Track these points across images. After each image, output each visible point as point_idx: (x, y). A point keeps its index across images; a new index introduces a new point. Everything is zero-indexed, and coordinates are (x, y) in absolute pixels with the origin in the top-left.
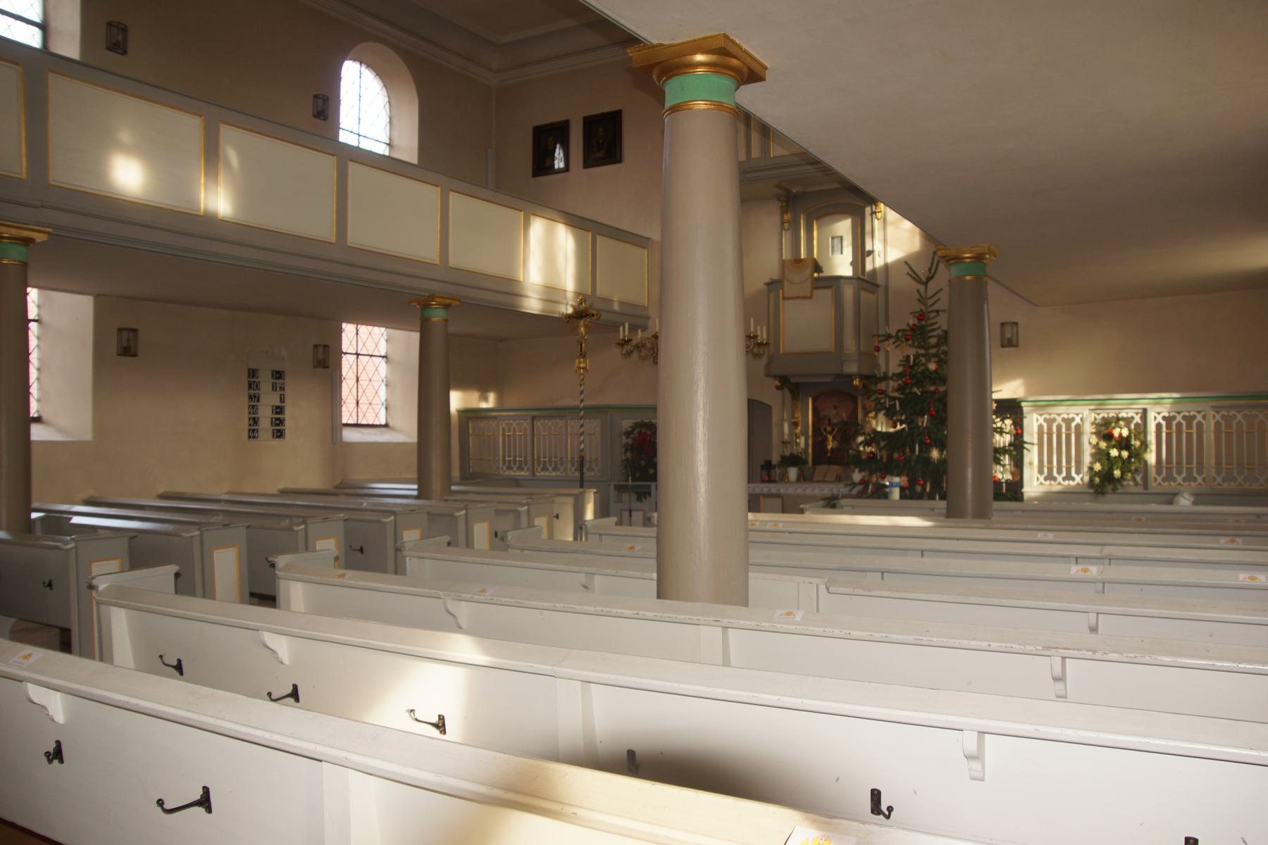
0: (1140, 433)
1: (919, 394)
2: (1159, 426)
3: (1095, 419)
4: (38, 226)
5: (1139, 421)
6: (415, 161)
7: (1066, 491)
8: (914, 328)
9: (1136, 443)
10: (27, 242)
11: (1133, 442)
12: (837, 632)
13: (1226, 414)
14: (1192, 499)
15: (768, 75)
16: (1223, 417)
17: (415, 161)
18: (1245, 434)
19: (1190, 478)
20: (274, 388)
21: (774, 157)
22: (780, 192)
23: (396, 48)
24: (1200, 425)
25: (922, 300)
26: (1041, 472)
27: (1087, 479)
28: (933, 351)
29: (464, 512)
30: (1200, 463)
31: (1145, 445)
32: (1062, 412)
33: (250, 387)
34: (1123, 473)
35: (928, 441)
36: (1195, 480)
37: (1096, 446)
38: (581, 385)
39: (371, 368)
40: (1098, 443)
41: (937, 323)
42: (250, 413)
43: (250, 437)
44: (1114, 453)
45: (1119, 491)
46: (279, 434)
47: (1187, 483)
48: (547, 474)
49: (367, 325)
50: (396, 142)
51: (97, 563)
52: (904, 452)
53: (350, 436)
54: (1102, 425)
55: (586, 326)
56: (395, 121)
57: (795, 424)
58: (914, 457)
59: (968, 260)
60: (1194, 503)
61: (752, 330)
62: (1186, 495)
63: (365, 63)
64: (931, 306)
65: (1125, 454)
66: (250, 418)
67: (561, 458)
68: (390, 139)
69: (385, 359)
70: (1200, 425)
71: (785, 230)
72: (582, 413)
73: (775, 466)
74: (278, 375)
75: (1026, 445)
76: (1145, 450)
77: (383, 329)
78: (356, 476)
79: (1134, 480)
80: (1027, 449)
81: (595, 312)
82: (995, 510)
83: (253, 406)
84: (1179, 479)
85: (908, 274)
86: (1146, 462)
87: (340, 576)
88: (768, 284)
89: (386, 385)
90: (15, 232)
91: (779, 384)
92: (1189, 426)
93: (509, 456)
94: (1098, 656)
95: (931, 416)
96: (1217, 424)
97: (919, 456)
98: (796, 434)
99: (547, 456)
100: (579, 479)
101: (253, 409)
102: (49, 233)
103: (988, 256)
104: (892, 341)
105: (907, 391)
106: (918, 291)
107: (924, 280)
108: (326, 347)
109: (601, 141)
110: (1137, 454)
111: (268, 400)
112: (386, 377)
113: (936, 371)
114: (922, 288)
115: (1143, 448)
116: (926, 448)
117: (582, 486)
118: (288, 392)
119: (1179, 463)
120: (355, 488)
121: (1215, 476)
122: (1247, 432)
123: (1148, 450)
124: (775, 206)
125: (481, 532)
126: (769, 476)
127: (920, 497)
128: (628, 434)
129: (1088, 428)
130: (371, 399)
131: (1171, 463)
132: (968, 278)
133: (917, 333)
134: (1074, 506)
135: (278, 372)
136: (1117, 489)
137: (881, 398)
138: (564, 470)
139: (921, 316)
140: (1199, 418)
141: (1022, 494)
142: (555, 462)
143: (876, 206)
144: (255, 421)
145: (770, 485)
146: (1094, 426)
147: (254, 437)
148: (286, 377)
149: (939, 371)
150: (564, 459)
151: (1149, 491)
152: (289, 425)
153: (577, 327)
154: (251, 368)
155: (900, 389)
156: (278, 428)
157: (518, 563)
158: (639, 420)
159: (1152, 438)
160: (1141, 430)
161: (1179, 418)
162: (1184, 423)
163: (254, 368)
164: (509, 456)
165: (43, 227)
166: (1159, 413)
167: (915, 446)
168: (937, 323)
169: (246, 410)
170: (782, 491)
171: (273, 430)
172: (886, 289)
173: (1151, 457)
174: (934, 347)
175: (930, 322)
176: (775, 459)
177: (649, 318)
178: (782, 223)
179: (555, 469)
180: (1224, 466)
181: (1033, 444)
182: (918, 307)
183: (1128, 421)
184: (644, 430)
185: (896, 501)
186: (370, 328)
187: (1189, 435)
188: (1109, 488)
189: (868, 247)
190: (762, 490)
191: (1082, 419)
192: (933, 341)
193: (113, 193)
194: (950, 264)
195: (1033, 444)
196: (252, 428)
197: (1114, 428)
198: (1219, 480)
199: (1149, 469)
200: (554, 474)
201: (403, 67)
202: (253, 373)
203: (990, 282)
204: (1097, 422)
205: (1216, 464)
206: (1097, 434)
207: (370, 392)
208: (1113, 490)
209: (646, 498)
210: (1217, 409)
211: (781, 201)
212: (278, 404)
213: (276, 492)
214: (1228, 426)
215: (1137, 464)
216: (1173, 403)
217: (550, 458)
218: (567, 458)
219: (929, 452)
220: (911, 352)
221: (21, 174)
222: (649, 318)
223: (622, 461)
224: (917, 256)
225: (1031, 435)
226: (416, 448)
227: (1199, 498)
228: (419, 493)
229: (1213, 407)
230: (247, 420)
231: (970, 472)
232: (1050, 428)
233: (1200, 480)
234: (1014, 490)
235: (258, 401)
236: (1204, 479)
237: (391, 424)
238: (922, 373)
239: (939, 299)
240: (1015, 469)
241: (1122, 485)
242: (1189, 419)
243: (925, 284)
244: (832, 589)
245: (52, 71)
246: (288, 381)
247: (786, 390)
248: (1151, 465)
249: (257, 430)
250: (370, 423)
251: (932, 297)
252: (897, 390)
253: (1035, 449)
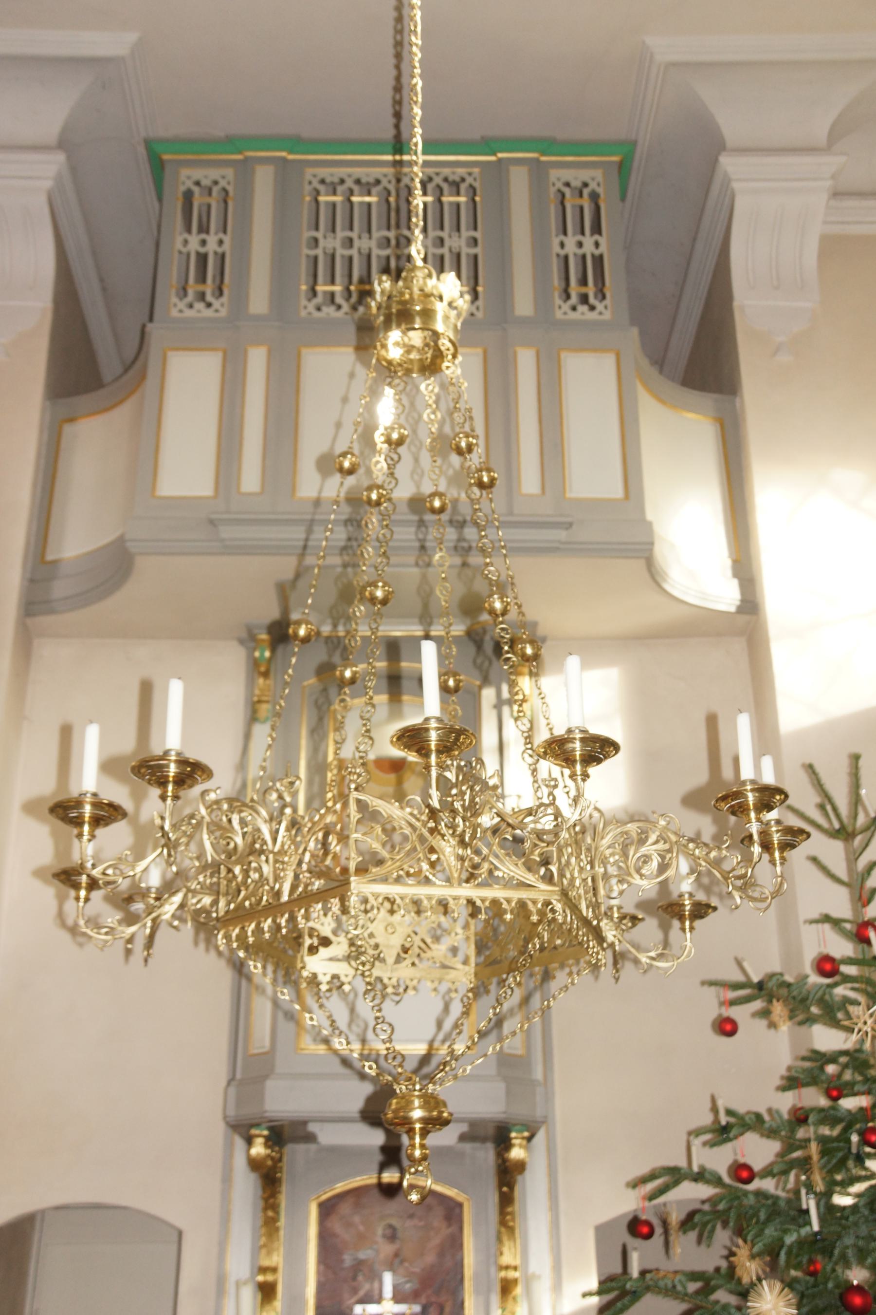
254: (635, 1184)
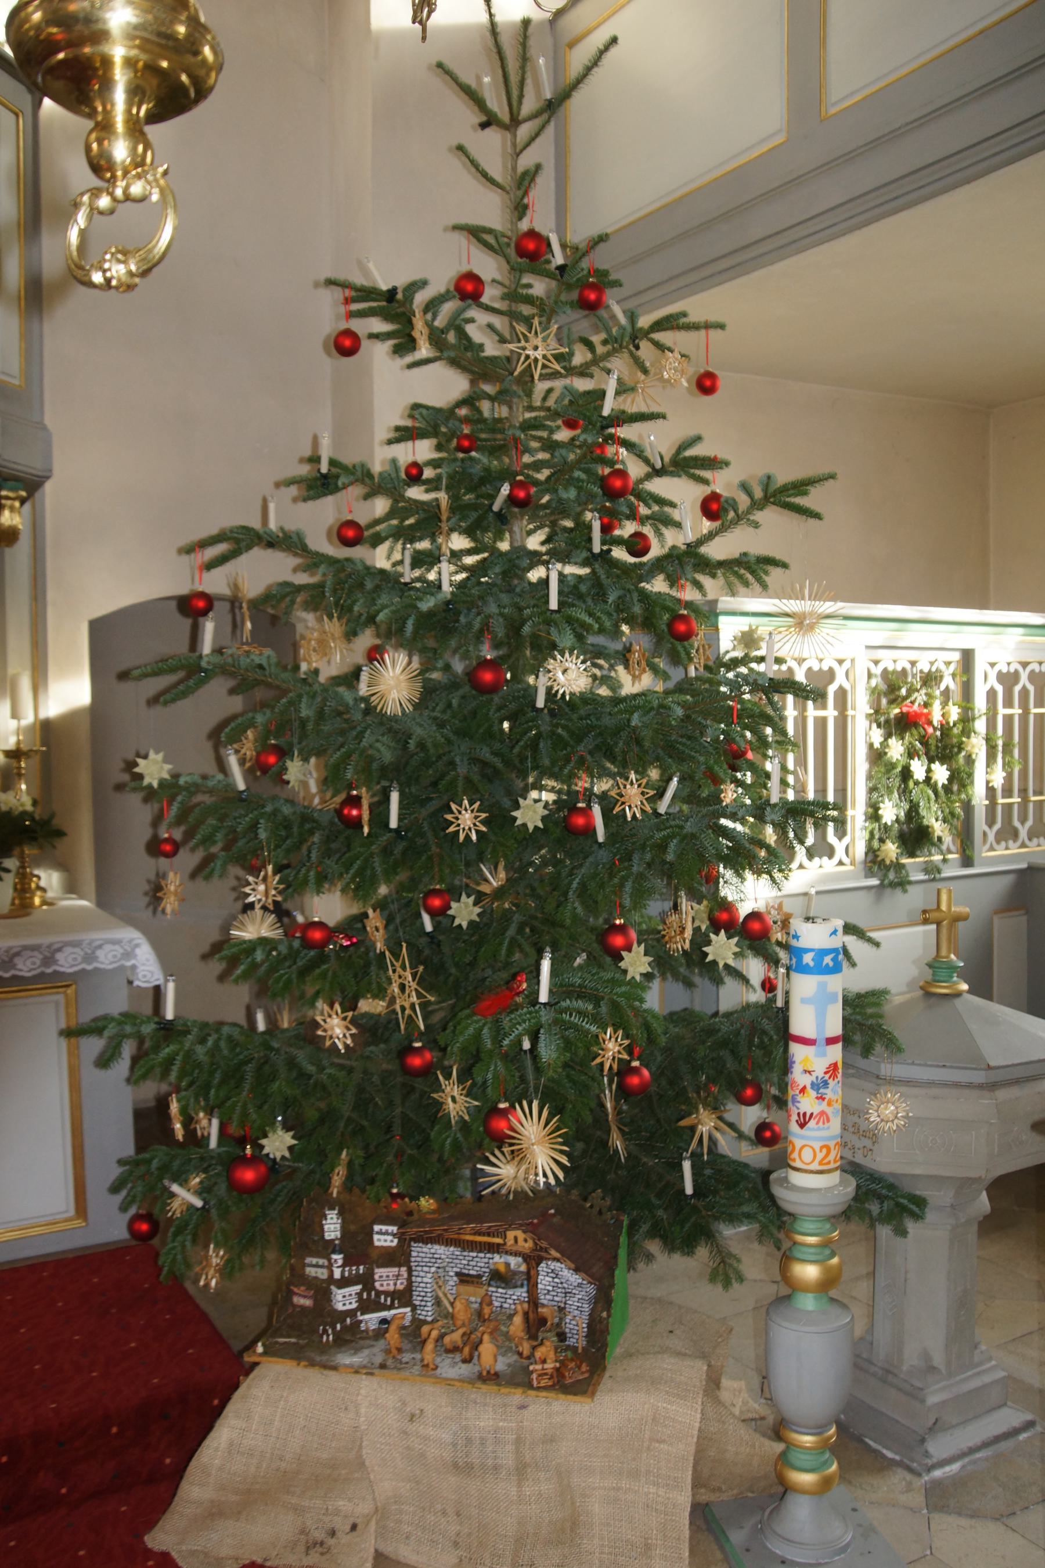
2: (991, 694)
27: (860, 850)
37: (877, 756)
40: (884, 744)
129: (861, 706)
166: (992, 665)
204: (874, 682)
206: (876, 716)
254: (189, 550)
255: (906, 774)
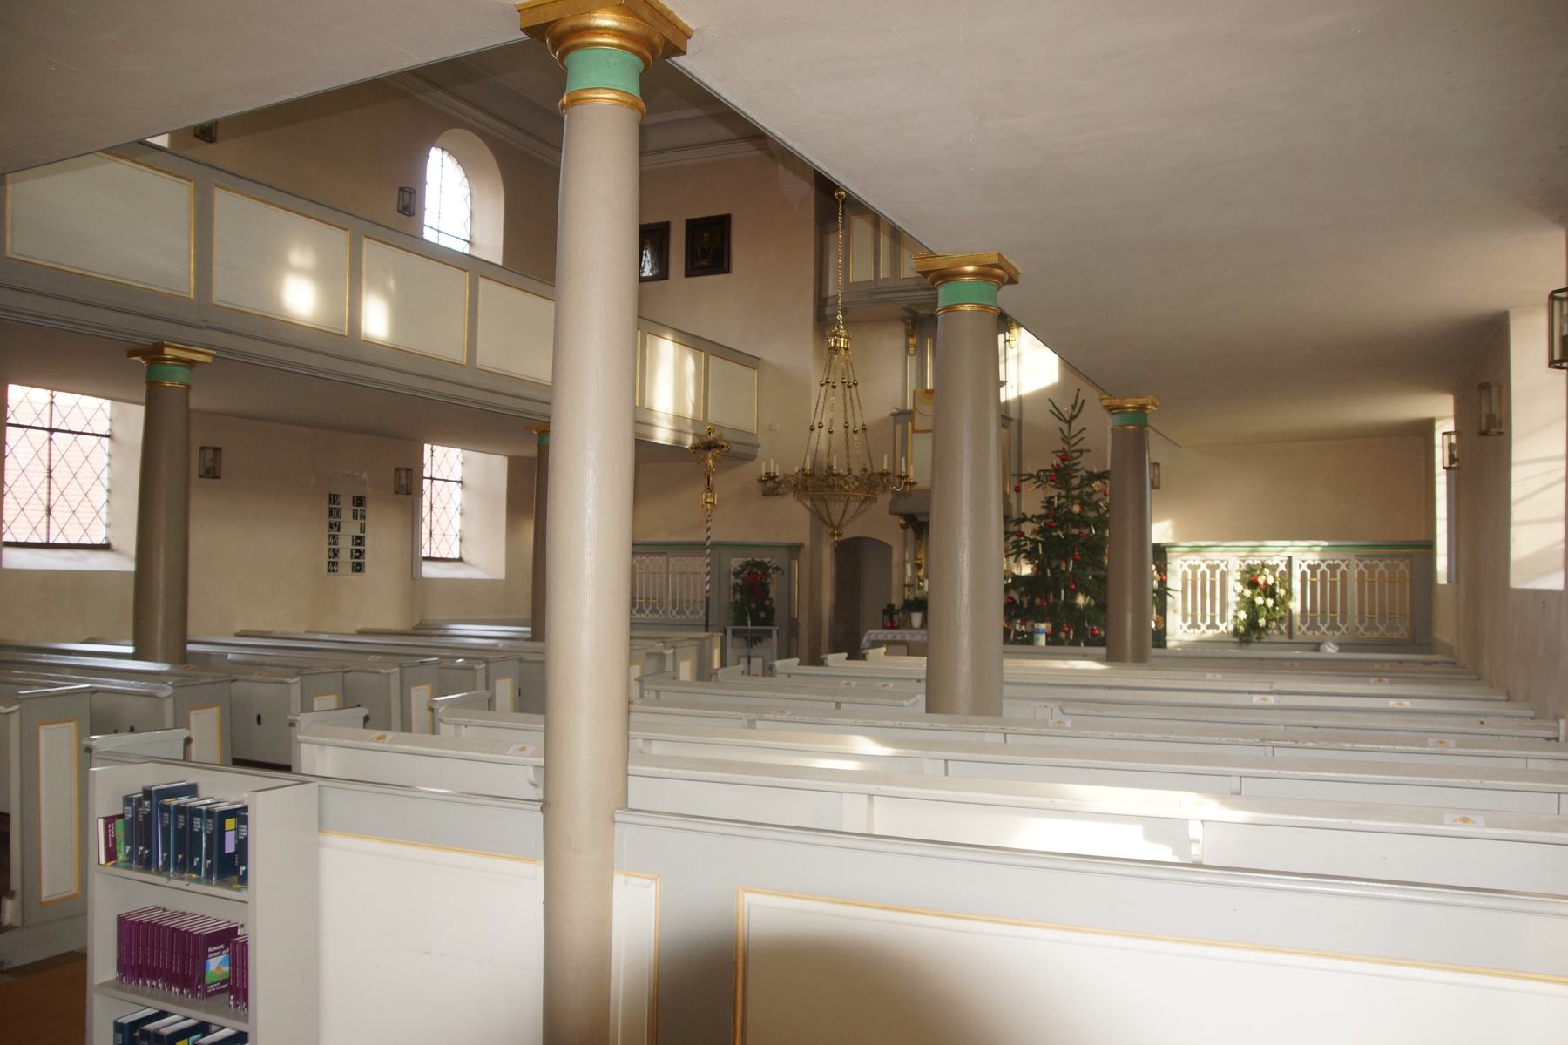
0: (1285, 581)
1: (1063, 537)
2: (1303, 574)
3: (1240, 566)
4: (203, 347)
5: (1285, 570)
6: (500, 262)
7: (1219, 639)
8: (1057, 469)
9: (1281, 592)
10: (190, 363)
11: (1277, 591)
12: (1103, 734)
13: (1369, 562)
14: (1337, 648)
15: (1021, 279)
16: (1366, 566)
17: (500, 262)
18: (1387, 584)
19: (1333, 627)
20: (355, 517)
21: (853, 283)
22: (907, 314)
23: (483, 135)
24: (1343, 573)
25: (1065, 439)
26: (1185, 620)
27: (1231, 628)
28: (1075, 493)
29: (672, 651)
30: (1344, 613)
31: (1289, 592)
32: (1214, 556)
33: (331, 514)
34: (1267, 622)
35: (1074, 587)
36: (1338, 629)
38: (708, 521)
39: (75, 456)
40: (1243, 591)
41: (1079, 463)
42: (330, 544)
43: (329, 571)
44: (1259, 601)
45: (1265, 640)
46: (359, 568)
47: (1331, 633)
48: (643, 616)
49: (442, 446)
50: (477, 240)
51: (319, 698)
52: (1047, 600)
53: (429, 571)
54: (1247, 572)
55: (714, 459)
56: (476, 216)
57: (918, 566)
58: (1060, 604)
59: (1130, 410)
60: (1339, 651)
61: (903, 469)
62: (1331, 645)
63: (447, 150)
64: (1074, 445)
65: (1270, 602)
66: (330, 549)
67: (660, 600)
68: (471, 237)
69: (460, 485)
70: (1343, 573)
71: (910, 355)
72: (708, 551)
73: (898, 610)
74: (359, 501)
75: (1170, 592)
76: (1290, 598)
77: (107, 404)
78: (435, 615)
79: (1279, 629)
80: (1171, 596)
81: (724, 444)
82: (1153, 657)
83: (334, 536)
84: (1323, 629)
85: (1051, 411)
86: (1290, 610)
87: (380, 738)
88: (893, 415)
89: (461, 514)
90: (181, 354)
91: (904, 522)
92: (1333, 575)
93: (641, 598)
94: (1300, 744)
95: (1075, 560)
96: (1361, 573)
97: (1064, 601)
98: (919, 577)
99: (644, 596)
100: (704, 623)
101: (333, 539)
102: (213, 355)
103: (1150, 407)
104: (1034, 480)
105: (1048, 534)
106: (1061, 429)
107: (1068, 418)
108: (409, 470)
109: (706, 248)
110: (1282, 602)
111: (349, 528)
112: (461, 505)
113: (1079, 514)
114: (1065, 427)
115: (1288, 595)
116: (1072, 594)
117: (707, 631)
118: (369, 521)
119: (1323, 612)
120: (433, 629)
121: (1358, 625)
122: (1389, 581)
123: (1293, 597)
124: (899, 330)
125: (686, 670)
126: (892, 621)
127: (1061, 643)
128: (737, 574)
130: (444, 529)
131: (1335, 612)
132: (1131, 427)
133: (1060, 474)
134: (1218, 652)
135: (359, 498)
136: (1261, 638)
137: (1021, 540)
138: (663, 612)
139: (1065, 457)
140: (1343, 566)
141: (1165, 642)
142: (640, 603)
143: (1010, 333)
144: (335, 552)
145: (895, 632)
146: (1239, 573)
147: (334, 571)
148: (367, 505)
149: (1083, 514)
150: (664, 601)
151: (1293, 641)
152: (368, 559)
153: (706, 458)
154: (333, 493)
155: (1041, 531)
156: (358, 560)
157: (768, 694)
158: (750, 559)
159: (1296, 585)
160: (1286, 577)
161: (1323, 566)
162: (1328, 571)
163: (335, 493)
164: (641, 598)
165: (208, 349)
166: (1304, 561)
167: (1060, 592)
168: (1079, 463)
169: (326, 540)
170: (908, 638)
171: (353, 563)
172: (1020, 422)
173: (1295, 606)
174: (1075, 488)
175: (1073, 462)
176: (897, 602)
177: (757, 446)
178: (907, 347)
179: (654, 611)
180: (1366, 615)
181: (1176, 591)
182: (1060, 445)
183: (1273, 569)
184: (755, 570)
185: (1042, 647)
186: (445, 449)
187: (1333, 584)
188: (1254, 636)
189: (1002, 378)
190: (876, 637)
191: (1226, 566)
192: (1075, 482)
193: (279, 315)
194: (1113, 414)
195: (1176, 591)
196: (331, 560)
197: (1259, 576)
198: (1362, 629)
199: (1293, 617)
200: (651, 616)
201: (490, 157)
202: (334, 499)
203: (1151, 432)
204: (1242, 569)
205: (1359, 613)
206: (1242, 581)
207: (74, 494)
208: (1257, 639)
209: (756, 644)
210: (1360, 558)
211: (907, 324)
212: (359, 534)
213: (355, 633)
214: (1371, 575)
215: (1283, 613)
216: (1322, 551)
217: (648, 599)
218: (667, 600)
219: (1074, 597)
220: (1054, 492)
221: (189, 294)
222: (757, 446)
223: (731, 603)
224: (1053, 389)
225: (1174, 582)
226: (132, 580)
227: (1342, 646)
228: (532, 636)
229: (1357, 556)
230: (326, 551)
231: (1129, 616)
232: (1194, 575)
233: (1343, 629)
234: (1160, 637)
235: (339, 530)
236: (1347, 629)
237: (465, 558)
238: (1065, 514)
239: (1082, 438)
240: (1158, 616)
241: (1267, 634)
242: (1333, 568)
243: (1069, 422)
244: (1067, 711)
245: (217, 186)
246: (370, 510)
247: (910, 530)
248: (1296, 615)
249: (337, 562)
250: (444, 556)
251: (1076, 435)
252: (1038, 533)
253: (1179, 596)
255: (1253, 602)
